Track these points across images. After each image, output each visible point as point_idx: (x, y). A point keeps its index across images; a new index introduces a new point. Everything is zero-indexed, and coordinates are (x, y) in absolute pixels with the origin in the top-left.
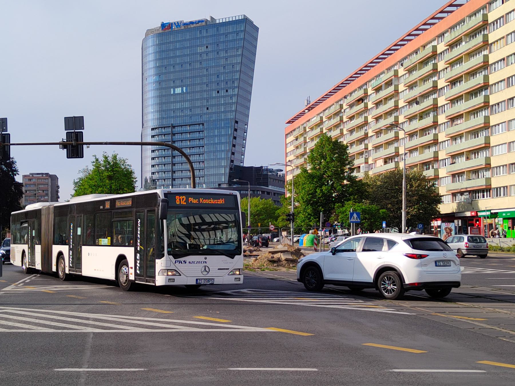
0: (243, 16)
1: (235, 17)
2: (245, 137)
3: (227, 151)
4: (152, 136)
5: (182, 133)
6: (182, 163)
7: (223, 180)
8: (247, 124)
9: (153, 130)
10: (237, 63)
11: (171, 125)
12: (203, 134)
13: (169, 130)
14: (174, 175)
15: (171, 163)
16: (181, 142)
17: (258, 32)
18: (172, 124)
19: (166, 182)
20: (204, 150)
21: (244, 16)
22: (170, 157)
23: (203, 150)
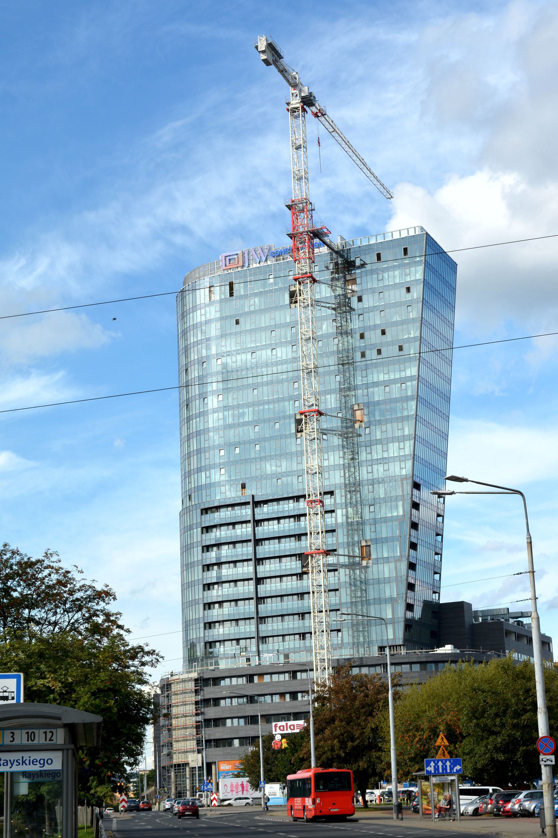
0: (417, 229)
1: (399, 232)
2: (439, 545)
3: (398, 560)
4: (205, 605)
5: (282, 616)
6: (283, 636)
7: (391, 636)
8: (439, 552)
9: (207, 513)
10: (409, 340)
11: (250, 500)
12: (334, 539)
13: (246, 512)
14: (261, 587)
15: (255, 635)
16: (278, 579)
17: (456, 272)
18: (253, 496)
19: (241, 589)
20: (342, 640)
21: (422, 229)
22: (250, 582)
23: (340, 639)
